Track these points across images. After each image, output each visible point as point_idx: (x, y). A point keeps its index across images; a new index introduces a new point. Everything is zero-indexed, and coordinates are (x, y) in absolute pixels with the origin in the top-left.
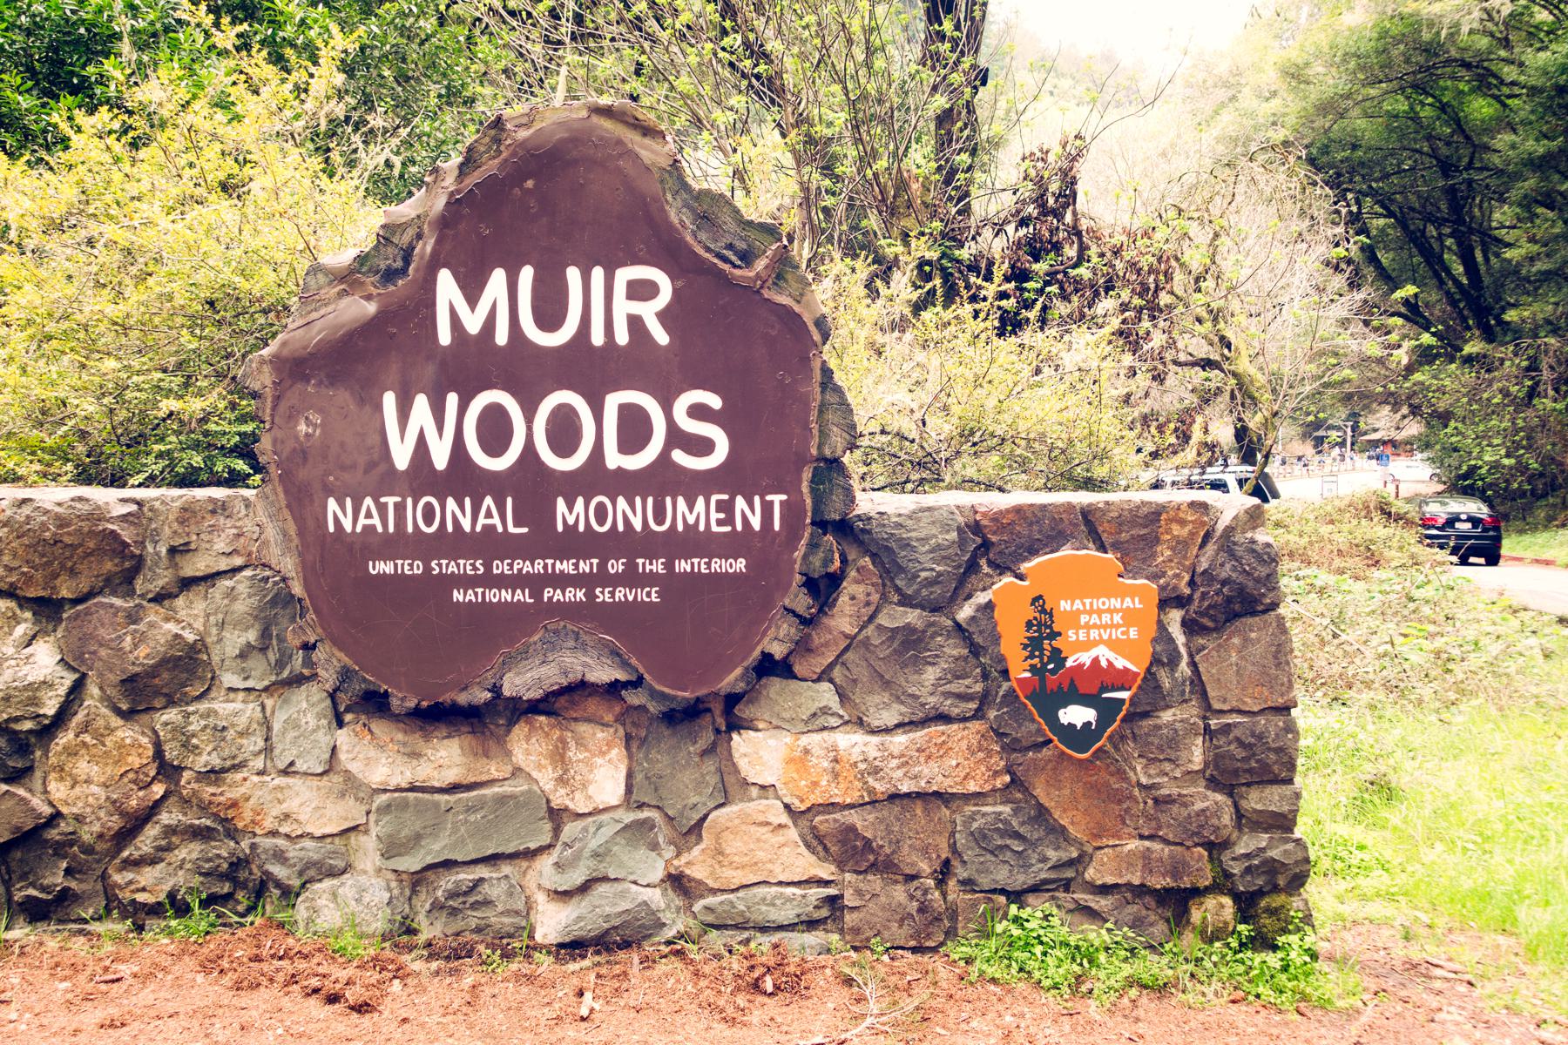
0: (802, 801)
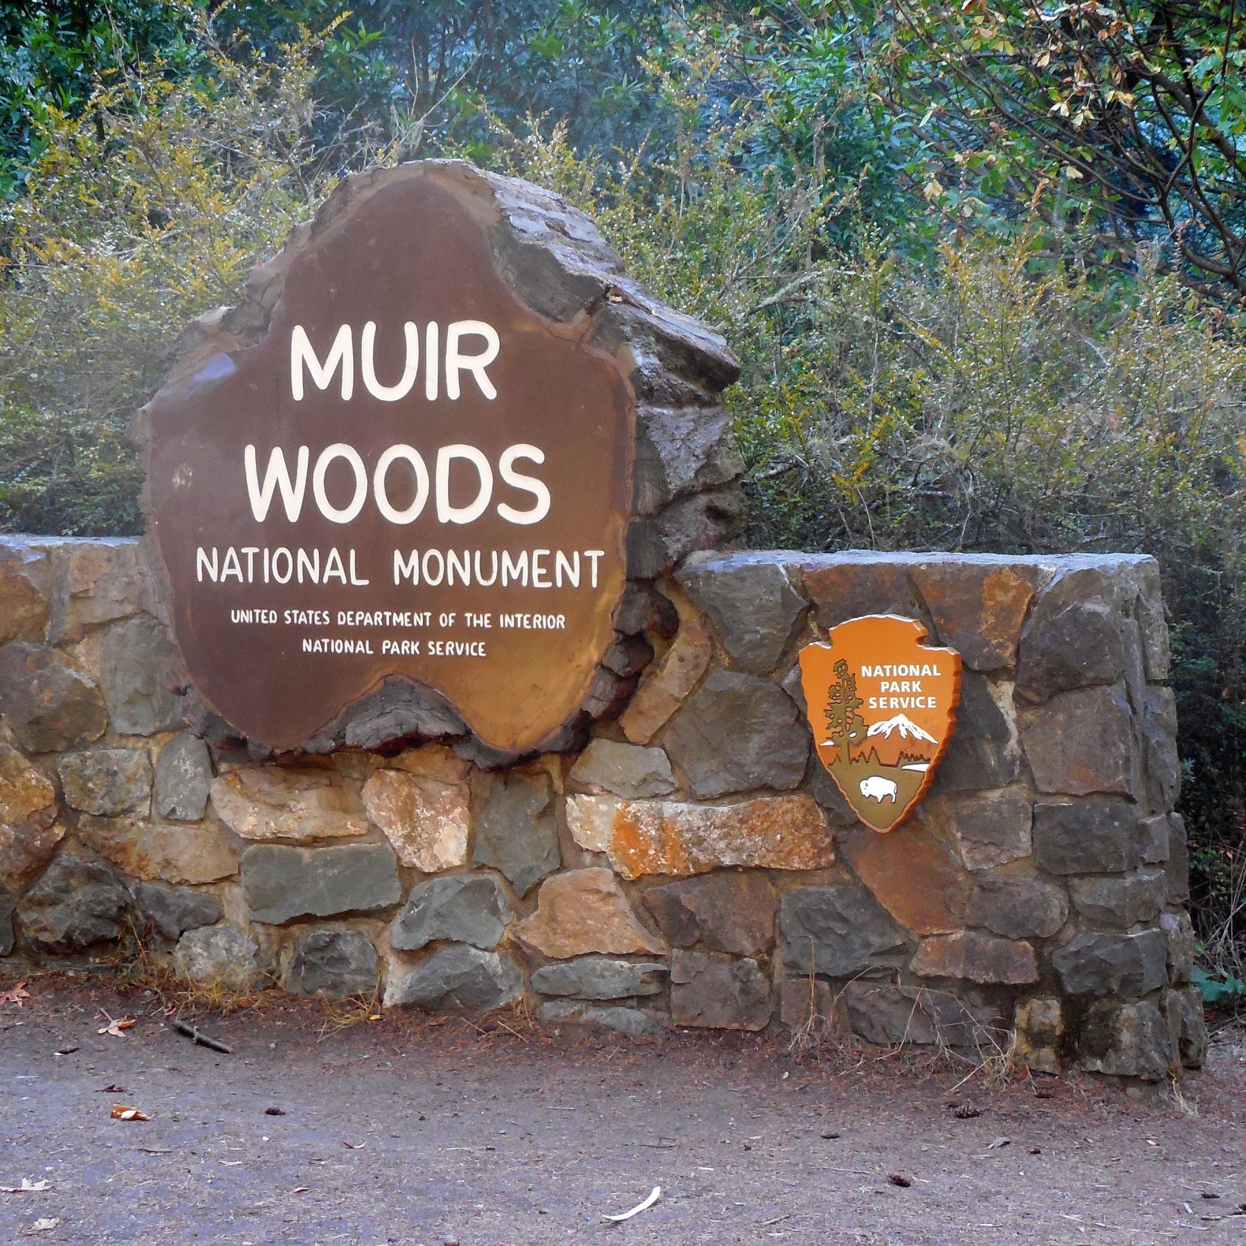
0: (632, 870)
